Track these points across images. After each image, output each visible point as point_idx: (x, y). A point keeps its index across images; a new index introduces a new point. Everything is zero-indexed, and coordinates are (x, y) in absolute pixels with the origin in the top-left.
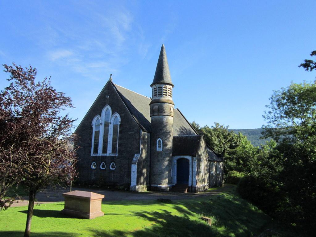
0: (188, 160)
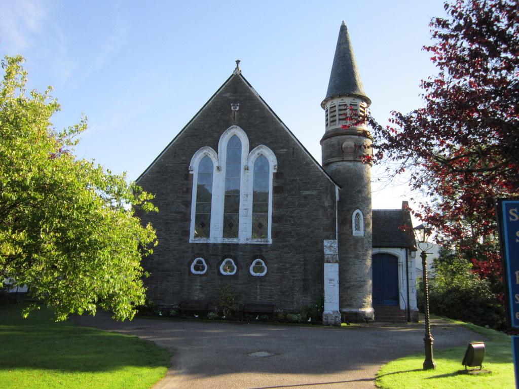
0: (395, 258)
